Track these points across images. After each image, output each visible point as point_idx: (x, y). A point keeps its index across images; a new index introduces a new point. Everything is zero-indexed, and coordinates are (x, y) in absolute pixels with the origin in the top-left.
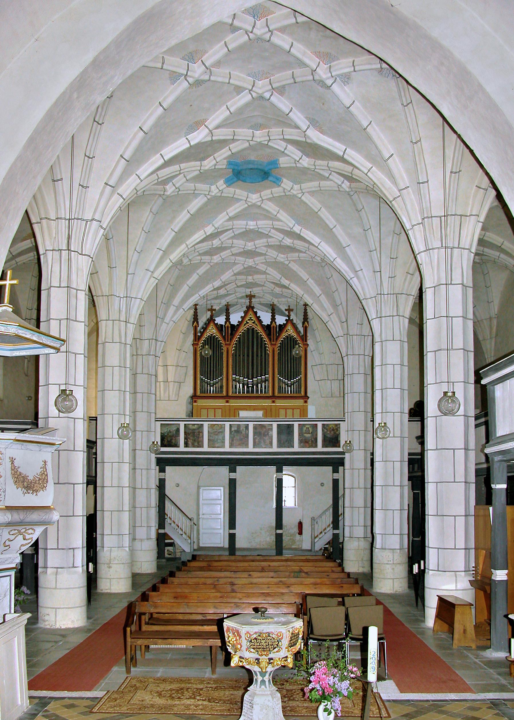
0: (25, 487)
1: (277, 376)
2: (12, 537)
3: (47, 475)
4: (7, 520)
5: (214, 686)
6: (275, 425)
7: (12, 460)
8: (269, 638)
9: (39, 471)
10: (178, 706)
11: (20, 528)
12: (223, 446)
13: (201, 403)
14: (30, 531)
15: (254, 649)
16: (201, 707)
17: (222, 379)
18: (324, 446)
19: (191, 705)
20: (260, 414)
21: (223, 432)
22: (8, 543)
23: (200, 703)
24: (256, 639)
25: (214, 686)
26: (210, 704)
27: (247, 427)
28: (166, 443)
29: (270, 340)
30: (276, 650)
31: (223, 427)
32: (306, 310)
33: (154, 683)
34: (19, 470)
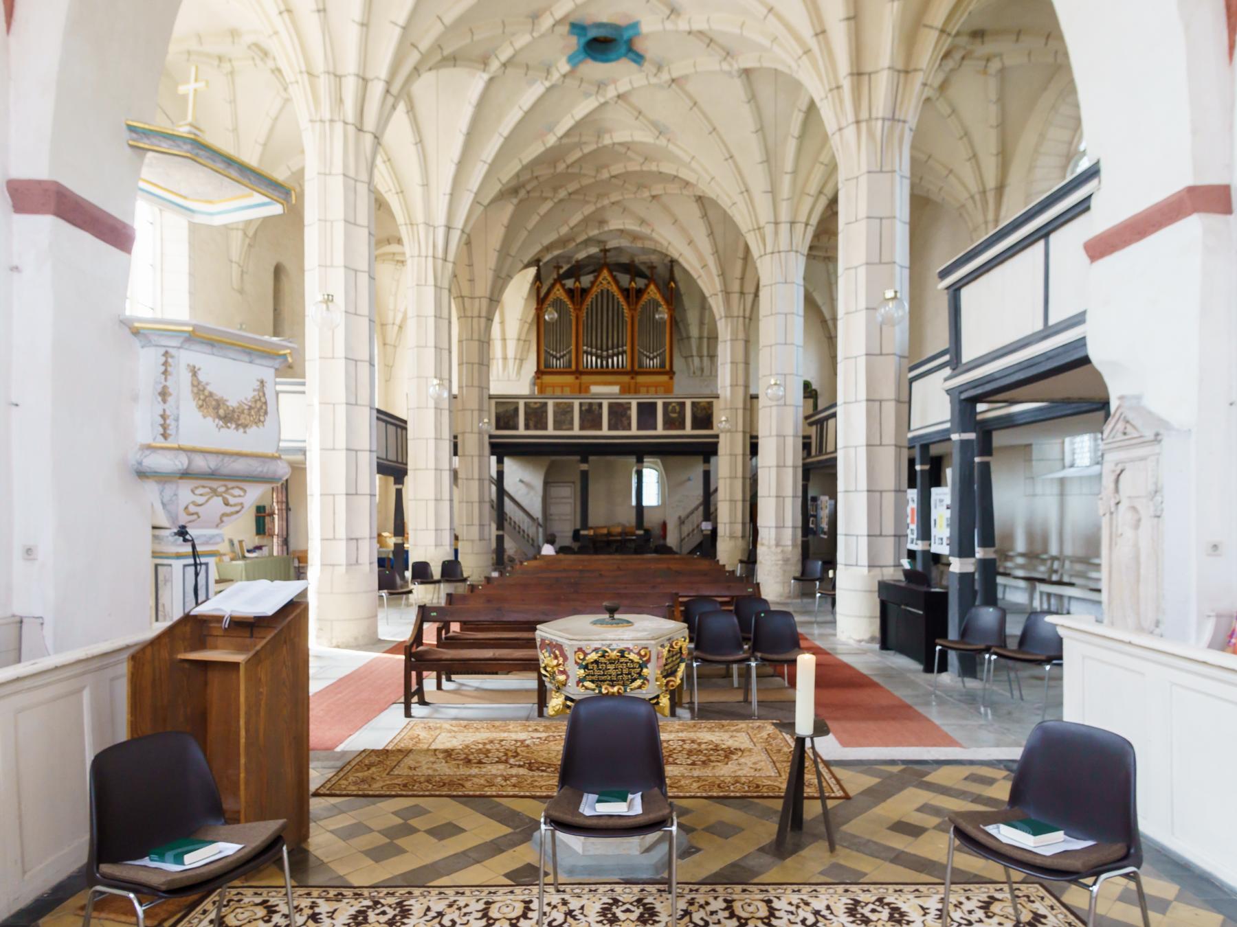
0: (220, 418)
1: (637, 348)
2: (200, 500)
3: (265, 403)
4: (180, 467)
5: (543, 735)
6: (634, 404)
7: (194, 372)
8: (623, 660)
9: (250, 394)
10: (475, 780)
11: (214, 484)
12: (572, 429)
13: (547, 379)
14: (237, 492)
15: (593, 681)
16: (514, 780)
17: (570, 352)
18: (694, 427)
19: (496, 776)
20: (616, 389)
21: (572, 411)
22: (192, 509)
23: (514, 771)
24: (596, 662)
25: (543, 735)
26: (531, 773)
27: (600, 405)
28: (502, 424)
29: (628, 303)
30: (638, 682)
31: (571, 406)
32: (672, 267)
33: (450, 731)
34: (209, 388)
